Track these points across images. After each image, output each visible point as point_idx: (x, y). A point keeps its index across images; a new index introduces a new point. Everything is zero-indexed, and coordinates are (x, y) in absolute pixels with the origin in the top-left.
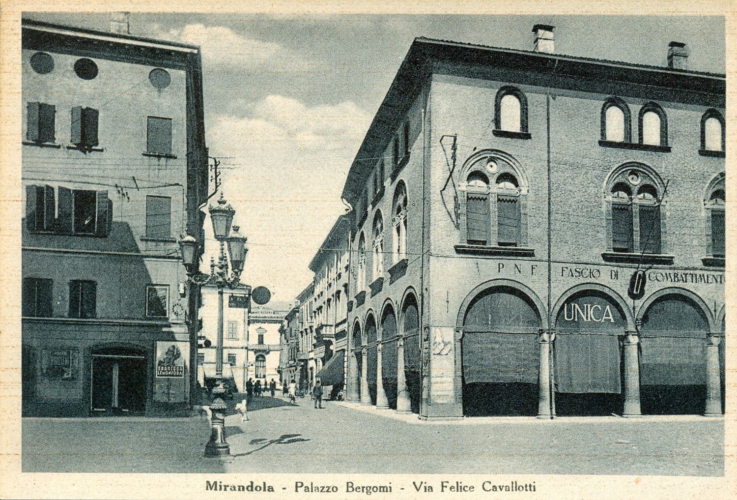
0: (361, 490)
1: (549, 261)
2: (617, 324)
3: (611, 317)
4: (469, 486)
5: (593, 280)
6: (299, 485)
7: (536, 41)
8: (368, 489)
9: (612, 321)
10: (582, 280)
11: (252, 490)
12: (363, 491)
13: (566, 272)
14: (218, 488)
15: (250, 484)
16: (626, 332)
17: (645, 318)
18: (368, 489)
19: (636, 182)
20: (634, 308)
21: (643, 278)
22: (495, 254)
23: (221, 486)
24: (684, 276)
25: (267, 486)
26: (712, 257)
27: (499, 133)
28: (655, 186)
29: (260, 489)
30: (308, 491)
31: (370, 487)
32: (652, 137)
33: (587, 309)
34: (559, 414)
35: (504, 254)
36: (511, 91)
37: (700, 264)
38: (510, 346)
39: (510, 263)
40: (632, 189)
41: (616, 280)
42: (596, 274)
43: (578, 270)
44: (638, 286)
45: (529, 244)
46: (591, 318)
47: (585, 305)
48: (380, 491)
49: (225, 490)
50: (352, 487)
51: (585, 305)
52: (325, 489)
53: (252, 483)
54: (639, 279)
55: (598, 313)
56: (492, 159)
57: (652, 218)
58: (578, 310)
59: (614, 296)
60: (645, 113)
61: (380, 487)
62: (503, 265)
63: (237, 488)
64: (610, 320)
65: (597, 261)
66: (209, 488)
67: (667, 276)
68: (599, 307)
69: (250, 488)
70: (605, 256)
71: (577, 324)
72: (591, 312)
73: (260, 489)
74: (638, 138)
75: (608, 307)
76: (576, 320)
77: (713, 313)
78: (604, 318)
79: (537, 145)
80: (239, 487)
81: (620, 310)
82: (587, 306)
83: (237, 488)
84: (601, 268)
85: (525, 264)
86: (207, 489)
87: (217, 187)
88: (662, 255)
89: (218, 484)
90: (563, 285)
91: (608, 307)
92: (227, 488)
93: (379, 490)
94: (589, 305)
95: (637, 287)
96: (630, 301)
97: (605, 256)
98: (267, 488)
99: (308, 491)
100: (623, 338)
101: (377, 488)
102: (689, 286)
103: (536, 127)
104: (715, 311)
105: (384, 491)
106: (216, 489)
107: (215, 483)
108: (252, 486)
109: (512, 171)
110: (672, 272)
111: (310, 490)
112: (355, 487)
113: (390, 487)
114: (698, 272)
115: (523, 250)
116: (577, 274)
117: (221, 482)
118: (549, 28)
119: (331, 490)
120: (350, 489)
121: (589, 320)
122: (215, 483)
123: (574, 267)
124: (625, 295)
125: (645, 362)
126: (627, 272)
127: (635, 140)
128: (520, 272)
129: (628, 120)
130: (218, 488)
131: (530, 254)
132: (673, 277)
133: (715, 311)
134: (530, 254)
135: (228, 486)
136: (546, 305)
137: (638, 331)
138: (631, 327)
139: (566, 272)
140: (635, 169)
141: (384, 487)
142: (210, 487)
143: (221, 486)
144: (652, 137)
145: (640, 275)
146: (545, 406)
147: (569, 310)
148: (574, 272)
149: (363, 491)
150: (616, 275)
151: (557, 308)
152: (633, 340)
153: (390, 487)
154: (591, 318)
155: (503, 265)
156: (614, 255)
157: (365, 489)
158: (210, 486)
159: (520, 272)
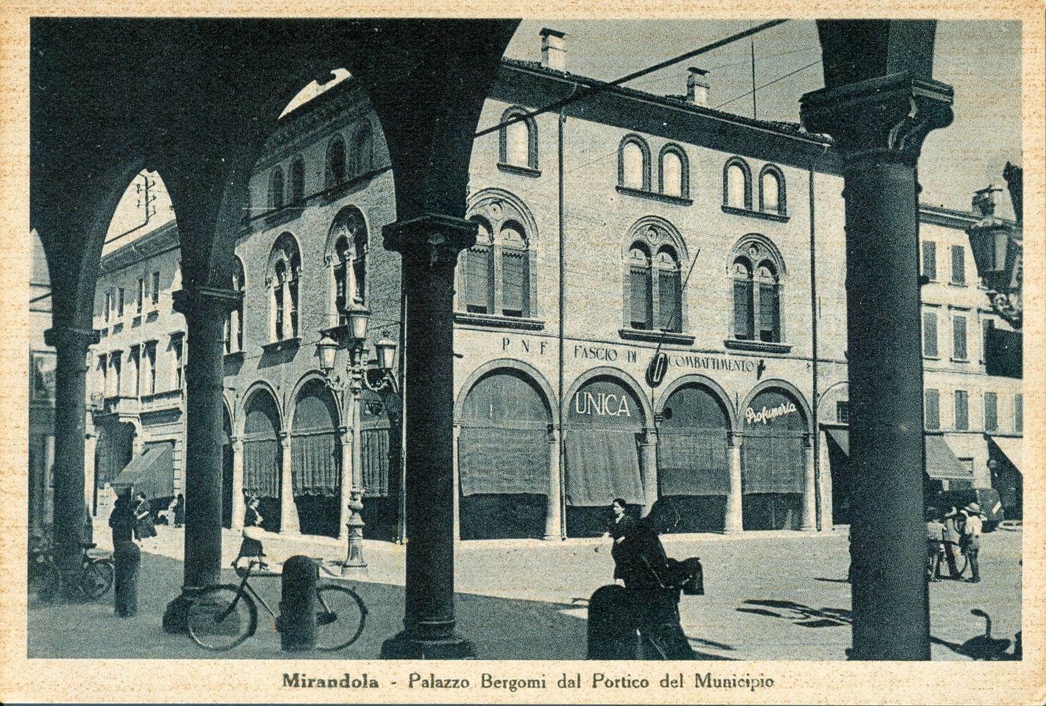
0: (502, 684)
1: (561, 337)
2: (632, 419)
3: (627, 410)
4: (640, 681)
5: (610, 363)
6: (415, 677)
7: (545, 49)
8: (513, 683)
9: (629, 415)
10: (598, 362)
11: (347, 686)
12: (505, 687)
13: (581, 351)
14: (300, 683)
15: (344, 678)
16: (643, 430)
17: (667, 413)
18: (513, 683)
19: (655, 242)
20: (653, 400)
21: (665, 361)
22: (500, 325)
23: (304, 681)
24: (705, 360)
25: (369, 679)
26: (735, 339)
27: (503, 167)
28: (675, 247)
29: (360, 685)
30: (428, 686)
31: (515, 681)
32: (673, 187)
33: (601, 400)
34: (570, 536)
35: (509, 326)
36: (527, 118)
37: (722, 347)
38: (514, 446)
39: (517, 338)
40: (652, 249)
41: (634, 363)
42: (613, 356)
43: (593, 350)
44: (658, 371)
45: (539, 315)
46: (606, 411)
47: (599, 394)
48: (529, 686)
49: (310, 685)
50: (489, 680)
51: (599, 394)
52: (452, 683)
53: (347, 675)
54: (660, 364)
55: (614, 405)
56: (498, 202)
57: (674, 284)
58: (591, 402)
59: (630, 382)
60: (667, 152)
61: (529, 681)
62: (509, 342)
63: (327, 683)
64: (626, 413)
65: (609, 339)
66: (699, 684)
67: (688, 360)
68: (614, 396)
69: (344, 683)
70: (622, 334)
71: (590, 417)
72: (605, 403)
73: (360, 685)
74: (639, 170)
75: (624, 397)
76: (589, 413)
77: (735, 407)
78: (620, 410)
79: (547, 182)
80: (330, 681)
81: (639, 403)
82: (601, 397)
83: (327, 683)
84: (619, 349)
85: (534, 340)
86: (285, 685)
87: (148, 218)
88: (683, 334)
89: (300, 677)
90: (579, 367)
91: (624, 397)
92: (314, 684)
93: (527, 685)
94: (604, 395)
95: (656, 371)
96: (647, 389)
97: (622, 334)
98: (369, 683)
99: (428, 686)
100: (641, 437)
101: (524, 682)
102: (709, 372)
103: (548, 161)
104: (737, 404)
105: (534, 687)
106: (297, 685)
107: (296, 676)
108: (347, 680)
109: (519, 219)
110: (693, 355)
111: (576, 685)
112: (493, 680)
113: (544, 681)
114: (719, 357)
115: (532, 322)
116: (592, 355)
117: (304, 675)
118: (560, 35)
119: (459, 684)
120: (487, 684)
121: (603, 413)
122: (296, 676)
123: (588, 345)
124: (642, 381)
125: (664, 466)
126: (646, 354)
127: (655, 189)
128: (527, 350)
129: (646, 162)
130: (300, 683)
131: (538, 327)
132: (694, 362)
133: (737, 404)
134: (538, 327)
135: (314, 681)
136: (557, 393)
137: (657, 429)
138: (650, 424)
139: (581, 351)
140: (655, 225)
141: (534, 681)
142: (289, 680)
143: (304, 681)
144: (673, 187)
145: (661, 359)
146: (555, 524)
147: (581, 401)
148: (588, 352)
149: (505, 687)
150: (634, 356)
151: (569, 399)
152: (651, 438)
153: (544, 681)
154: (606, 411)
155: (509, 342)
156: (632, 332)
157: (507, 684)
158: (291, 681)
159: (527, 350)
